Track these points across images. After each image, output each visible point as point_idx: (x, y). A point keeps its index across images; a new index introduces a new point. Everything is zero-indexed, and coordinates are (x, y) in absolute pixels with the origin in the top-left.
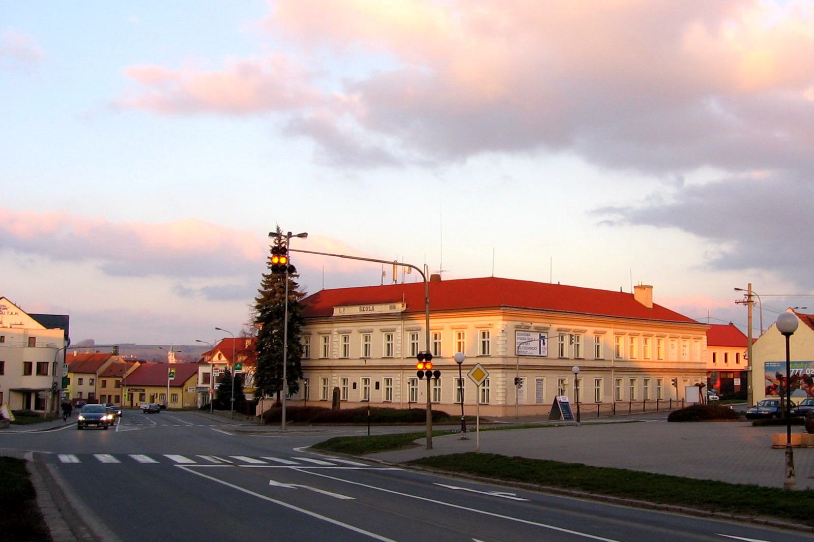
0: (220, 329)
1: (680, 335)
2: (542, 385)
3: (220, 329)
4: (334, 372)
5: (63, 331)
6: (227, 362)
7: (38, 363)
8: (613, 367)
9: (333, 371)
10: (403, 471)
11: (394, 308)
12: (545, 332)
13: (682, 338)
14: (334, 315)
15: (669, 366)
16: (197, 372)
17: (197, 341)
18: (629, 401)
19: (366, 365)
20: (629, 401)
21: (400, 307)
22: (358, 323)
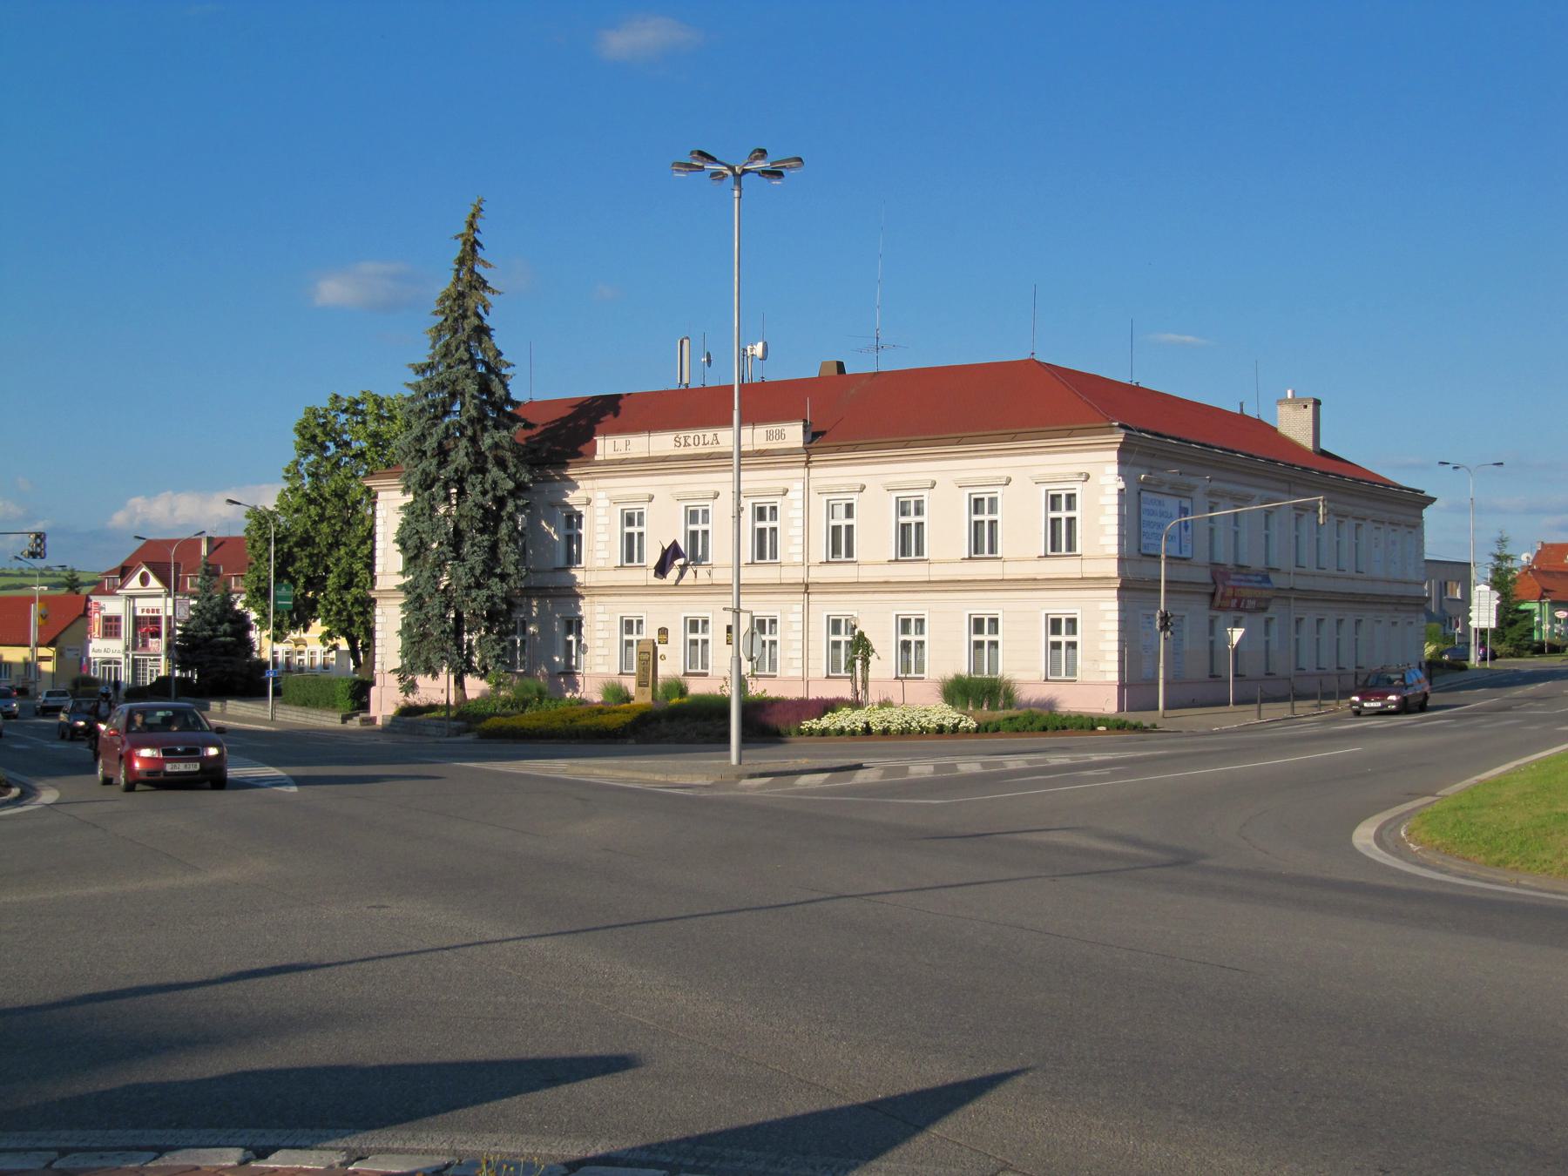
0: (239, 504)
1: (1349, 509)
2: (1182, 631)
3: (239, 504)
4: (600, 603)
5: (742, 449)
6: (163, 591)
7: (1420, 500)
8: (1292, 589)
9: (596, 599)
10: (942, 803)
11: (781, 435)
12: (1189, 497)
13: (1374, 521)
14: (597, 458)
15: (1380, 589)
16: (86, 613)
17: (1036, 483)
18: (1354, 670)
19: (698, 583)
20: (1354, 670)
21: (794, 434)
22: (766, 472)
